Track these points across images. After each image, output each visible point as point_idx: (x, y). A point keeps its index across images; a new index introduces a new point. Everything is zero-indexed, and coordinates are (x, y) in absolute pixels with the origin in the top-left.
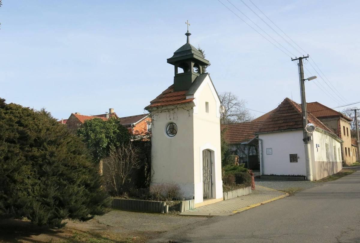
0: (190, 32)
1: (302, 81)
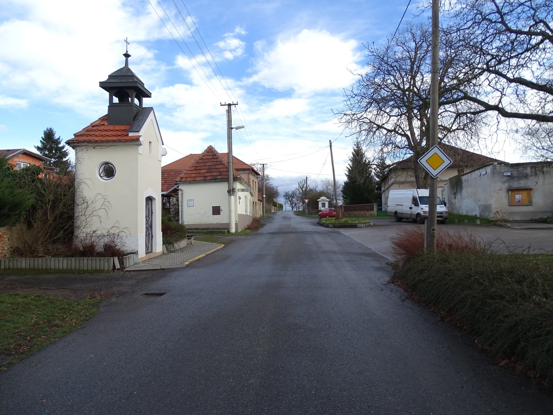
0: (129, 53)
1: (230, 128)
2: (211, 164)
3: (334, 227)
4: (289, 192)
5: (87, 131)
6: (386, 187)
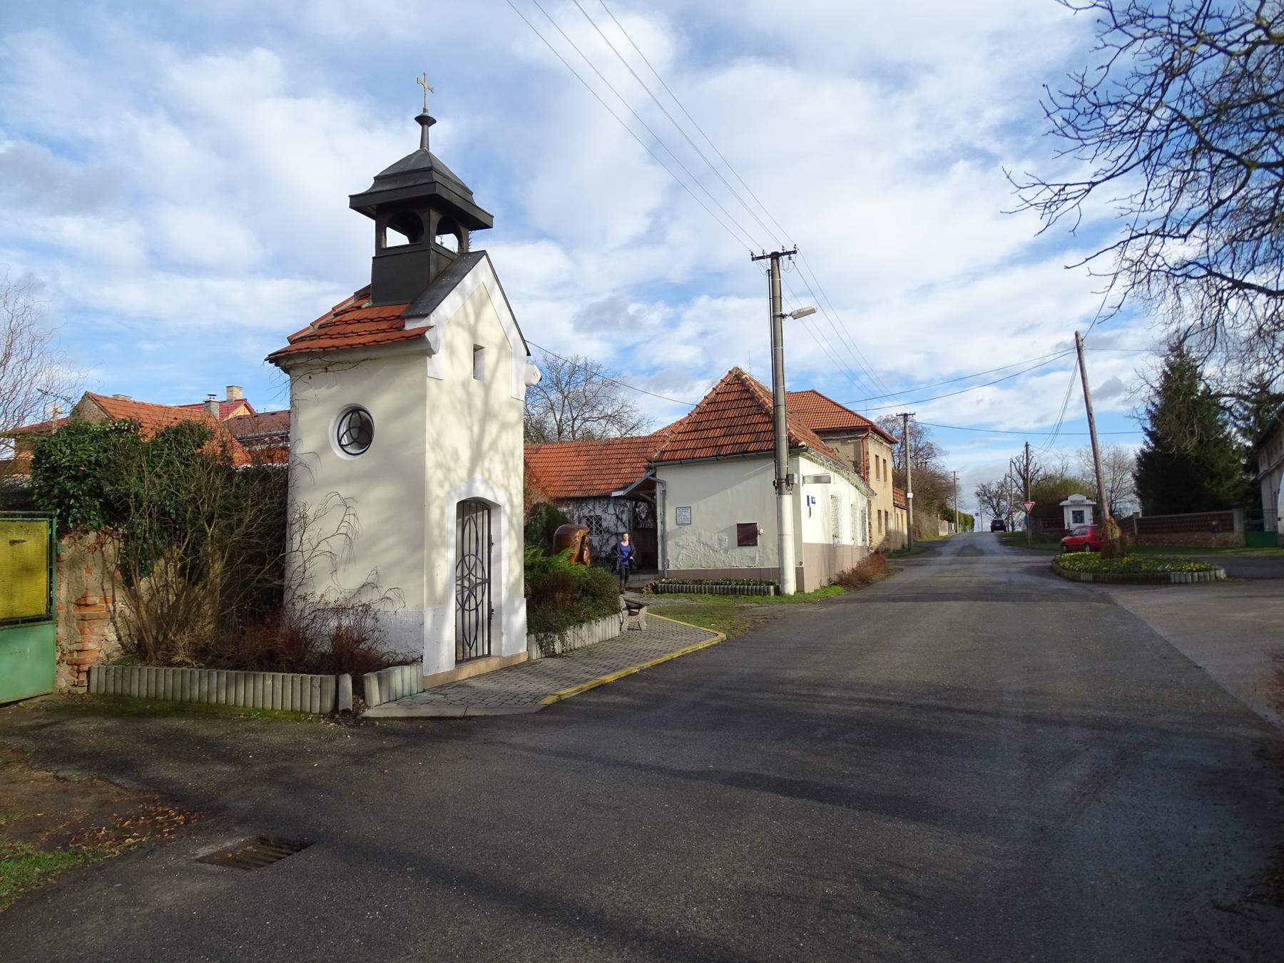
0: (429, 114)
1: (777, 317)
2: (736, 413)
3: (1096, 581)
4: (990, 484)
5: (320, 327)
6: (1275, 461)
